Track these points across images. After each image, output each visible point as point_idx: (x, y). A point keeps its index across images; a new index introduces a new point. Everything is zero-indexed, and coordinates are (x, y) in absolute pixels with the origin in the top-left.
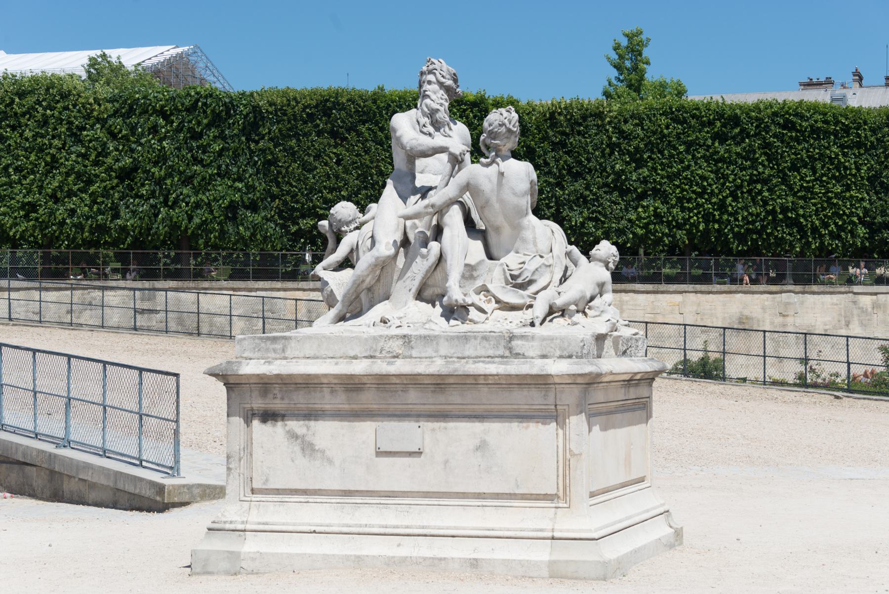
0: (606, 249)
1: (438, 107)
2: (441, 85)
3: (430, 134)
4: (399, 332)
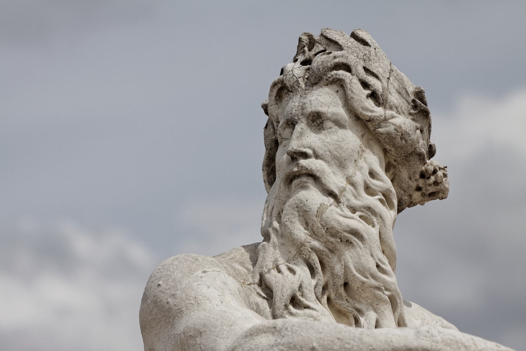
1: (355, 222)
2: (365, 124)
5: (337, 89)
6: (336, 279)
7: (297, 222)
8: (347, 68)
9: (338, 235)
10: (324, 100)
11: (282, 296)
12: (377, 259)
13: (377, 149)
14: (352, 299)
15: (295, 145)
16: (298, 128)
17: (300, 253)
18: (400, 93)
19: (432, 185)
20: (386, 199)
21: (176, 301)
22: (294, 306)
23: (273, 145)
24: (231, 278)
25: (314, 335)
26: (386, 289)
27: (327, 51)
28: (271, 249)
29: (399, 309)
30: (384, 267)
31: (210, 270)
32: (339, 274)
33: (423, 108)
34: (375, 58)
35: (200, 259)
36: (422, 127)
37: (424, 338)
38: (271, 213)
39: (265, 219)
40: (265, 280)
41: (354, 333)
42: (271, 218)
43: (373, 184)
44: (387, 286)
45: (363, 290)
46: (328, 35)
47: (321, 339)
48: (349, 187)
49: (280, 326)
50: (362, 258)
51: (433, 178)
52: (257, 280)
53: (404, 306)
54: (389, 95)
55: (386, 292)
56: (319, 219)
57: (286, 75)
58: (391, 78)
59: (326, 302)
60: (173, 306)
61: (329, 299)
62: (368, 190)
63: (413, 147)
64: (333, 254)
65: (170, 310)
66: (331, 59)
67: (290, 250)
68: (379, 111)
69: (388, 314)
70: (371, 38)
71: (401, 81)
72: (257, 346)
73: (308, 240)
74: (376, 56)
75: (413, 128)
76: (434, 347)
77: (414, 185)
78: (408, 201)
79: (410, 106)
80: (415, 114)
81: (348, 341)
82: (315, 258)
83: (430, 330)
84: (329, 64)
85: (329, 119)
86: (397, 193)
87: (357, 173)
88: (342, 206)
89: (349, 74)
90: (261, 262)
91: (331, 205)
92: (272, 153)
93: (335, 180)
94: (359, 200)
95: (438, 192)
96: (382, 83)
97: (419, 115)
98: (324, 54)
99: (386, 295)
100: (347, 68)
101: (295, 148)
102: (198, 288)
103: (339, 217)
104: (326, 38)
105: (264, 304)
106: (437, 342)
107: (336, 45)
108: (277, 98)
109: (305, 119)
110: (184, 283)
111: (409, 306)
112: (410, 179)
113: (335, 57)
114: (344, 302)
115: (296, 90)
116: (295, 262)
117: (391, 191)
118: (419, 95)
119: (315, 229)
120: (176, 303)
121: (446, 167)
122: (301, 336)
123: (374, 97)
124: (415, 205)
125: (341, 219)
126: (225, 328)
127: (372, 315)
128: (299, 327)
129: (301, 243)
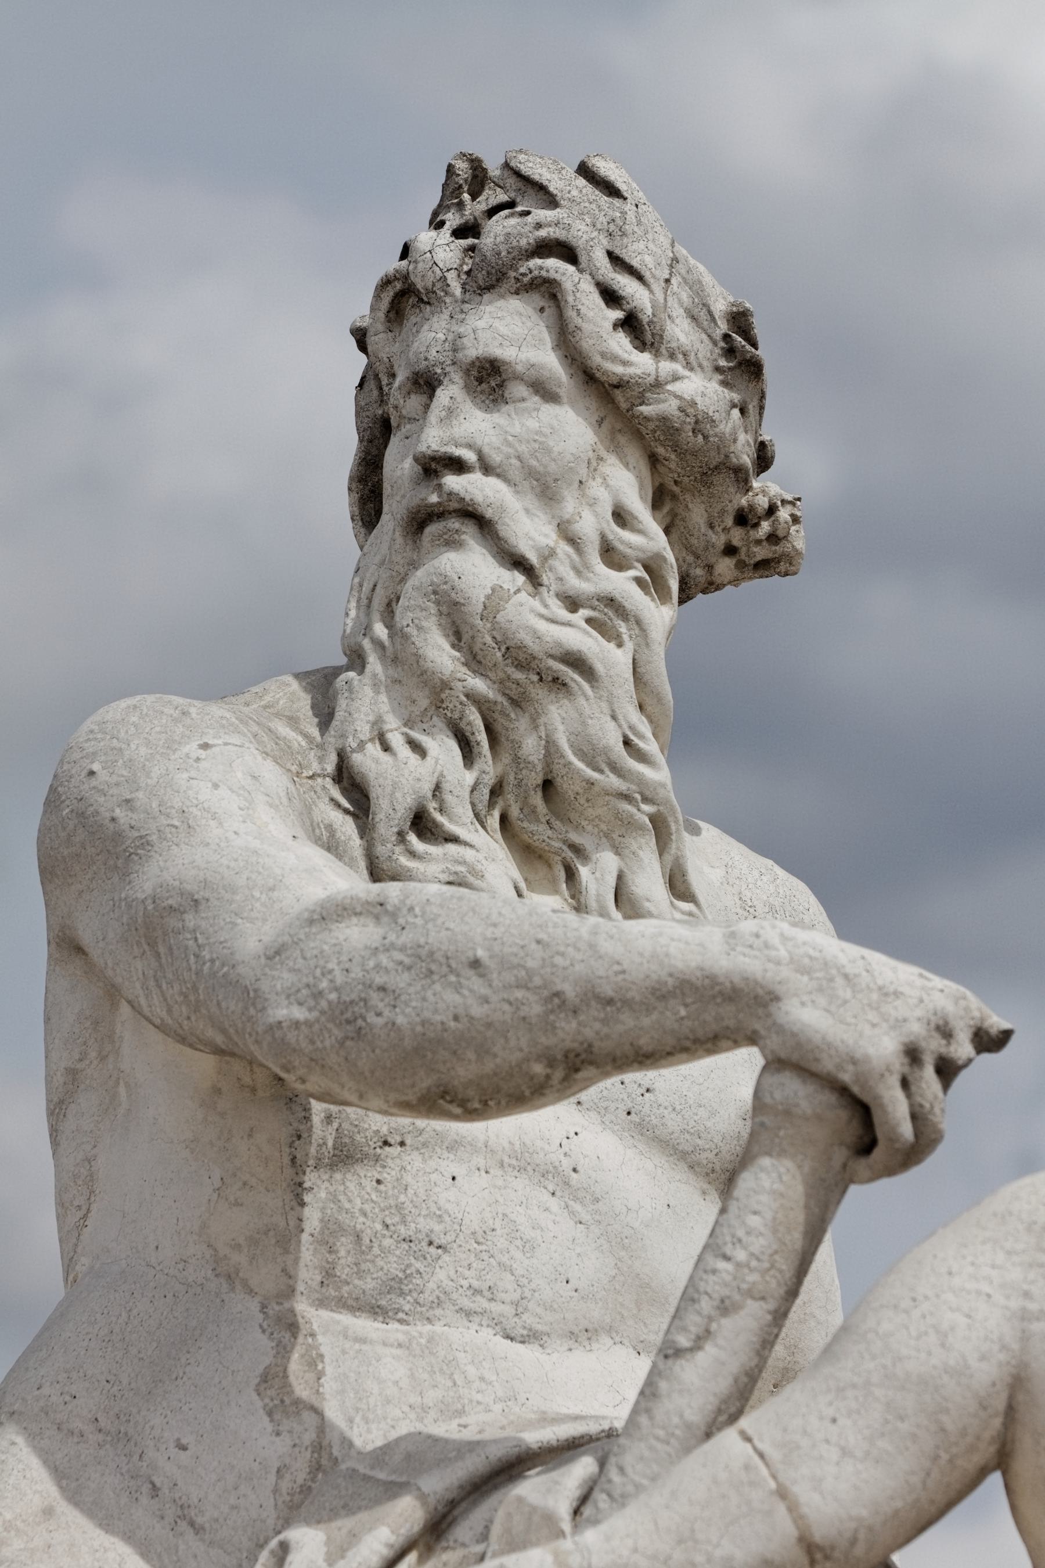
1: (578, 636)
2: (607, 395)
5: (542, 304)
6: (524, 772)
7: (434, 628)
8: (568, 253)
9: (533, 665)
10: (508, 330)
11: (391, 811)
12: (625, 726)
13: (635, 454)
14: (562, 820)
15: (434, 438)
16: (442, 396)
17: (438, 705)
18: (694, 318)
19: (764, 543)
20: (653, 577)
21: (135, 816)
22: (421, 835)
23: (377, 433)
24: (269, 764)
25: (479, 930)
26: (646, 800)
27: (519, 209)
28: (368, 691)
29: (674, 845)
30: (641, 744)
31: (220, 742)
32: (531, 758)
33: (748, 356)
34: (636, 229)
35: (193, 711)
36: (745, 402)
37: (747, 951)
38: (370, 600)
39: (353, 613)
40: (350, 768)
41: (576, 930)
42: (368, 614)
43: (622, 542)
44: (647, 793)
45: (588, 801)
46: (522, 167)
47: (495, 939)
48: (564, 548)
49: (396, 901)
50: (590, 722)
51: (765, 526)
52: (330, 767)
53: (685, 834)
54: (668, 322)
55: (645, 808)
56: (489, 625)
57: (416, 262)
58: (673, 281)
59: (497, 825)
60: (126, 827)
61: (504, 819)
62: (610, 554)
63: (723, 451)
64: (518, 710)
65: (118, 836)
66: (527, 228)
67: (414, 696)
68: (642, 364)
69: (646, 861)
70: (626, 177)
71: (696, 287)
72: (337, 949)
73: (459, 675)
74: (639, 223)
75: (724, 406)
76: (769, 975)
77: (719, 540)
78: (703, 580)
79: (717, 351)
80: (730, 369)
81: (562, 949)
82: (474, 718)
83: (762, 932)
84: (523, 242)
85: (518, 378)
86: (677, 560)
87: (583, 514)
88: (545, 594)
89: (571, 268)
90: (342, 722)
91: (518, 591)
92: (374, 452)
93: (529, 529)
94: (588, 580)
95: (777, 560)
96: (651, 292)
97: (738, 372)
98: (512, 215)
99: (643, 812)
100: (568, 253)
101: (434, 447)
102: (189, 788)
103: (539, 621)
104: (518, 174)
105: (347, 828)
106: (778, 963)
107: (542, 193)
108: (391, 315)
109: (461, 374)
110: (156, 772)
111: (695, 831)
112: (711, 526)
113: (539, 226)
114: (542, 828)
115: (440, 300)
116: (425, 726)
117: (665, 560)
118: (740, 321)
119: (476, 649)
120: (133, 823)
121: (799, 499)
122: (447, 929)
123: (630, 326)
124: (718, 588)
125: (542, 626)
126: (257, 894)
127: (608, 862)
128: (441, 906)
129: (442, 680)
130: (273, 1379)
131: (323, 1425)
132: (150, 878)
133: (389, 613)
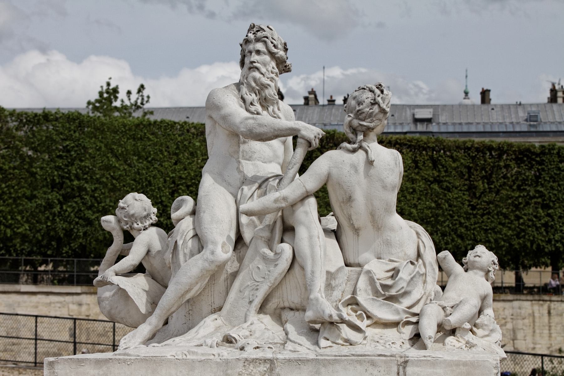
0: (482, 255)
1: (268, 82)
2: (272, 55)
3: (258, 114)
4: (259, 354)
8: (267, 38)
13: (275, 61)
15: (252, 59)
62: (272, 72)
68: (275, 50)
71: (281, 40)
93: (263, 70)
100: (267, 38)
103: (265, 81)
105: (243, 104)
118: (285, 44)
127: (272, 107)
130: (238, 168)
131: (244, 174)
132: (223, 112)
133: (247, 78)
